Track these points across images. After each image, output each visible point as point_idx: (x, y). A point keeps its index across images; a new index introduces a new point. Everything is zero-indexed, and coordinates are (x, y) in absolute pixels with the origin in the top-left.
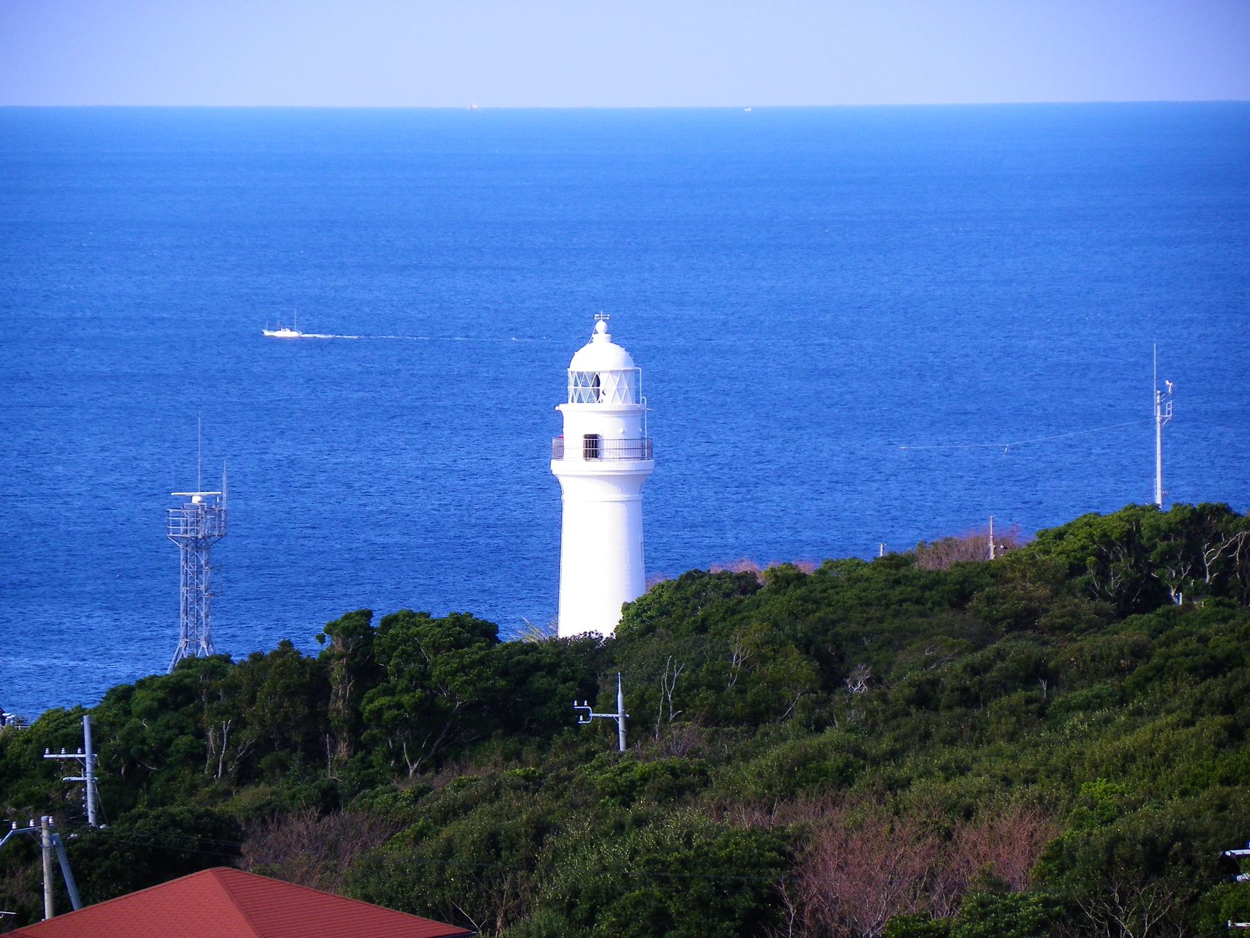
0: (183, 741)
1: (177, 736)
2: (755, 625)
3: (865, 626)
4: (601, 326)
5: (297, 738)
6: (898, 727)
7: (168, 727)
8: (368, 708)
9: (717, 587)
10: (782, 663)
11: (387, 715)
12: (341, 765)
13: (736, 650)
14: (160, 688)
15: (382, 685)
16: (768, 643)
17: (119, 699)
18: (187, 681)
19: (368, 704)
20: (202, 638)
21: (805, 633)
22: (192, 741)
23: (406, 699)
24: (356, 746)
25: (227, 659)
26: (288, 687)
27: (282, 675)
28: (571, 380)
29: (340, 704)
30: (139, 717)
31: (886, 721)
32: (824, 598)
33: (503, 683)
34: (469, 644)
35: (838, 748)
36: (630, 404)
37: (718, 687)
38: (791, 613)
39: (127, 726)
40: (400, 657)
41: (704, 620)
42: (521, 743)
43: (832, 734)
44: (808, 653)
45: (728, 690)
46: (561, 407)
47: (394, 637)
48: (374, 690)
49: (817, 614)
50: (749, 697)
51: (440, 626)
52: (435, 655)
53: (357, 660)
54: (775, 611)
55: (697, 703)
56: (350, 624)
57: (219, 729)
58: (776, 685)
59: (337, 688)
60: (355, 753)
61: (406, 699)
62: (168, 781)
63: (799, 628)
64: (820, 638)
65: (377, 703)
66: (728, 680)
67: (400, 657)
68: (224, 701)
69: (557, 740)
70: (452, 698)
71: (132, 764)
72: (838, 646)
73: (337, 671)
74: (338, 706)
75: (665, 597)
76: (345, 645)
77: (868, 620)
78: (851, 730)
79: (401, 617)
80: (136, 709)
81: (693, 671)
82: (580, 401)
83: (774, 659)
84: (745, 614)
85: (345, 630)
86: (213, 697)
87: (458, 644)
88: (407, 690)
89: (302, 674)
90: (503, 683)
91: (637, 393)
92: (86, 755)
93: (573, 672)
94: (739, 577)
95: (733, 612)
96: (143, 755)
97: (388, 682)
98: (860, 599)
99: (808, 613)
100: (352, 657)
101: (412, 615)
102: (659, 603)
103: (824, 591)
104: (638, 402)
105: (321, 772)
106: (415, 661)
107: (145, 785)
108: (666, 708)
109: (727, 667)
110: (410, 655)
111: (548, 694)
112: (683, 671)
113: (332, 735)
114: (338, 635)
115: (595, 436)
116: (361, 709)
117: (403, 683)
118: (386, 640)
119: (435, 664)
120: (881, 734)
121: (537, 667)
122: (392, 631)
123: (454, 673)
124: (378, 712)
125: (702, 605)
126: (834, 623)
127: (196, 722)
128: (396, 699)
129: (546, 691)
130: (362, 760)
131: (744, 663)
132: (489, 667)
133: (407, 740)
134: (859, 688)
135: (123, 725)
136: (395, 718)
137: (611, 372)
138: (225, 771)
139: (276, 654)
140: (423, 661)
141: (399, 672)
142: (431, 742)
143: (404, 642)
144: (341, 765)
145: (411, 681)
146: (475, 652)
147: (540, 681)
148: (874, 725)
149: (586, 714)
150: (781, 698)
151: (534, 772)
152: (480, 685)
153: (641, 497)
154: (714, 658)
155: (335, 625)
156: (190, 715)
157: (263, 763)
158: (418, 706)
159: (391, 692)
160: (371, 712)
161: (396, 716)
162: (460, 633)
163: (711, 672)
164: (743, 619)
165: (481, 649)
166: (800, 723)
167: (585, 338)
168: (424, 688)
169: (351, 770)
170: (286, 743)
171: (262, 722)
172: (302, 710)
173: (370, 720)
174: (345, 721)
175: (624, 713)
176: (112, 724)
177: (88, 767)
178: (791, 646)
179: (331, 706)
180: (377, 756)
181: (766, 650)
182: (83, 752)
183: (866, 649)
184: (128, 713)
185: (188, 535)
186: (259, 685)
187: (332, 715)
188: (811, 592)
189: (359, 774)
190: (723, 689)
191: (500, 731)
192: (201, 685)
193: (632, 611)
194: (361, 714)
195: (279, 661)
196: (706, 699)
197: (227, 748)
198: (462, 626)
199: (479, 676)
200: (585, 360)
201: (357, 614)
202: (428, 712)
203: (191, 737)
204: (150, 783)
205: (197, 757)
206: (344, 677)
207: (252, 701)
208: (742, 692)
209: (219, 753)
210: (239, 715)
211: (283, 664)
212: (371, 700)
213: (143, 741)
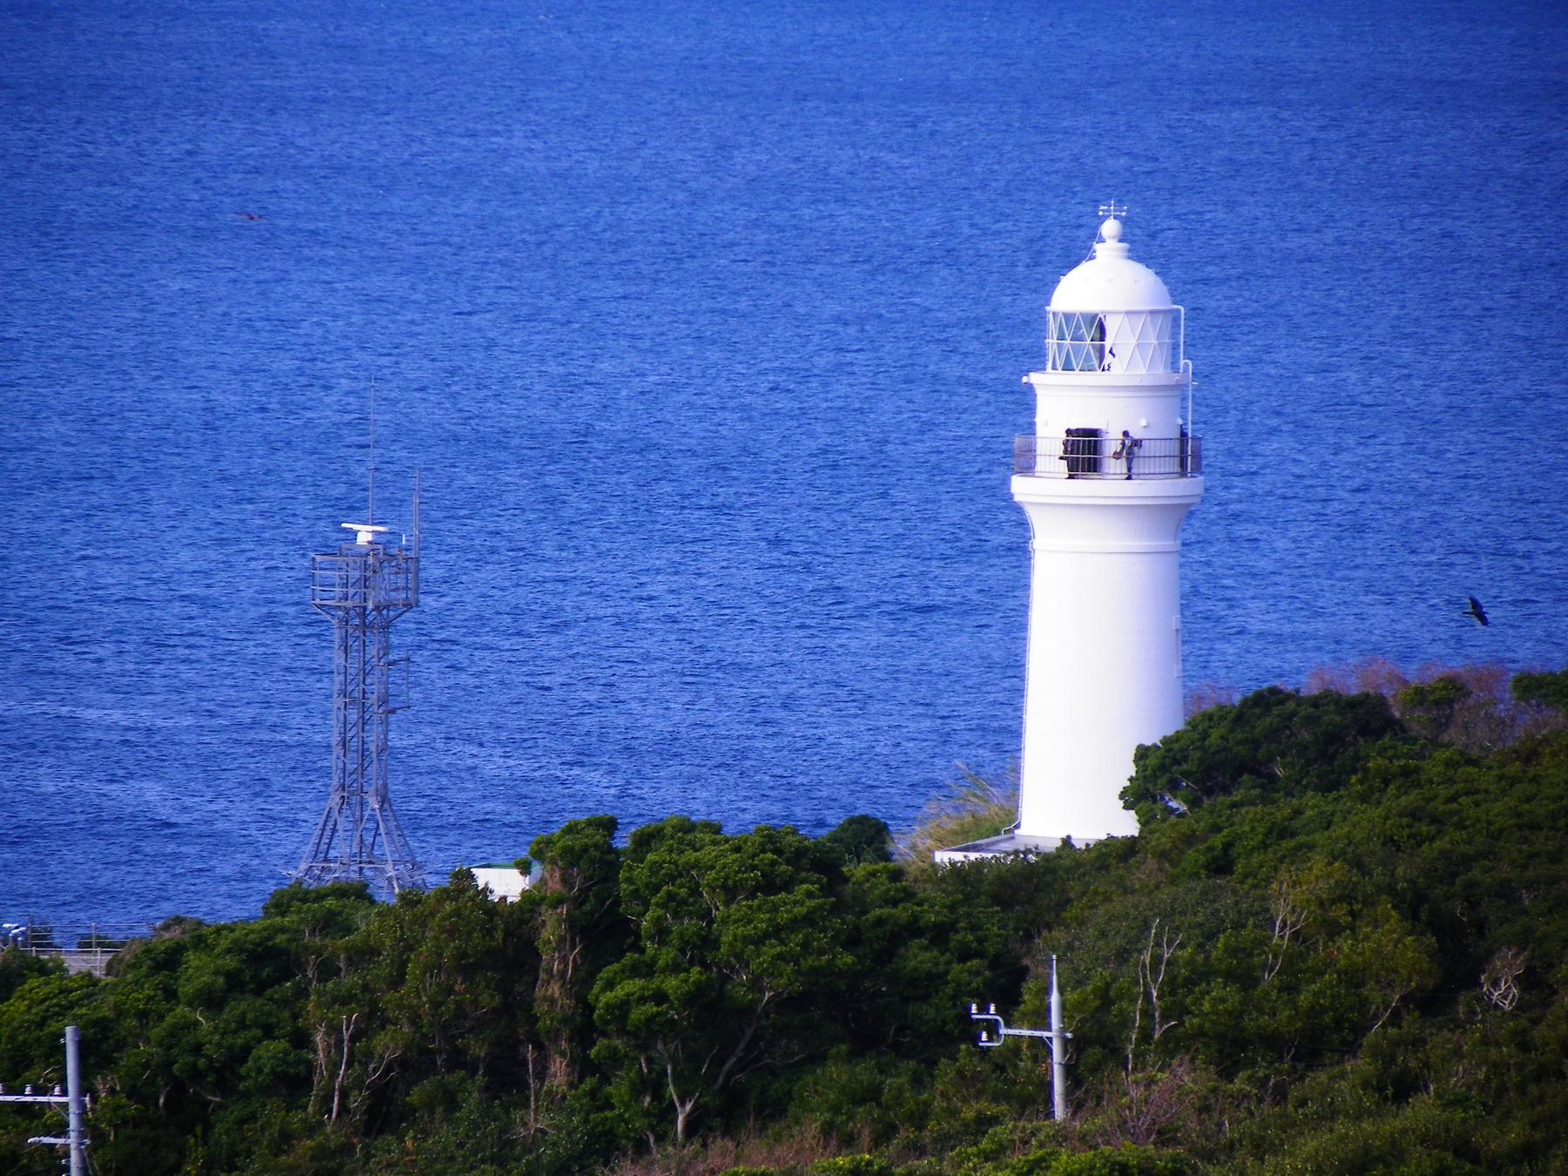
0: (269, 1052)
1: (259, 1041)
2: (1318, 863)
3: (1525, 867)
4: (1110, 228)
5: (478, 1049)
6: (1541, 1099)
7: (242, 1025)
8: (603, 999)
9: (1310, 721)
10: (1367, 938)
11: (637, 1014)
12: (555, 1102)
13: (1281, 911)
14: (229, 951)
15: (630, 957)
16: (1340, 899)
17: (157, 967)
18: (281, 939)
19: (603, 990)
20: (372, 790)
21: (1413, 882)
22: (286, 1053)
23: (672, 984)
24: (583, 1067)
25: (360, 893)
26: (464, 955)
27: (452, 933)
28: (1052, 326)
29: (555, 989)
30: (190, 1004)
31: (1521, 1089)
32: (1451, 814)
33: (849, 959)
34: (787, 886)
35: (1426, 1140)
36: (1161, 374)
37: (1245, 979)
38: (1389, 841)
39: (169, 1020)
40: (663, 905)
41: (1228, 846)
42: (881, 1072)
43: (1422, 1110)
44: (1415, 917)
45: (1263, 986)
46: (1034, 378)
47: (655, 868)
48: (616, 967)
49: (1437, 844)
50: (1304, 999)
51: (738, 849)
52: (727, 904)
53: (587, 907)
54: (1358, 835)
55: (1206, 1006)
56: (577, 842)
57: (334, 1030)
58: (1354, 978)
59: (551, 961)
60: (581, 1079)
61: (672, 984)
62: (241, 1122)
63: (1400, 871)
64: (1439, 891)
65: (620, 992)
66: (1264, 966)
67: (663, 905)
68: (349, 980)
69: (946, 1071)
70: (756, 984)
71: (178, 1086)
72: (1473, 904)
73: (551, 929)
74: (551, 994)
75: (1215, 737)
76: (566, 881)
77: (1532, 856)
78: (1459, 1102)
79: (668, 831)
80: (186, 989)
81: (1201, 946)
82: (1067, 367)
83: (1353, 929)
84: (1302, 839)
85: (567, 851)
86: (328, 970)
87: (769, 885)
88: (675, 968)
89: (489, 933)
90: (849, 959)
91: (1175, 347)
92: (67, 1099)
93: (980, 941)
94: (1354, 704)
95: (1284, 833)
96: (196, 1075)
97: (642, 951)
98: (1519, 816)
99: (1419, 840)
100: (579, 901)
101: (687, 827)
102: (1202, 748)
103: (1453, 799)
104: (1176, 370)
105: (517, 1115)
106: (690, 914)
107: (199, 1130)
108: (1147, 1014)
109: (1262, 943)
110: (684, 902)
111: (936, 979)
112: (1182, 946)
113: (539, 1047)
114: (553, 862)
115: (1093, 433)
116: (591, 998)
117: (667, 955)
118: (641, 873)
119: (724, 922)
120: (1508, 1115)
121: (913, 929)
122: (650, 857)
123: (759, 941)
124: (623, 1007)
125: (1283, 755)
126: (1467, 861)
127: (295, 1017)
128: (655, 983)
129: (931, 976)
130: (593, 1094)
131: (1295, 936)
132: (824, 930)
133: (673, 1059)
134: (1503, 993)
135: (161, 1018)
136: (651, 1019)
137: (1128, 313)
138: (343, 1109)
139: (444, 895)
140: (706, 915)
141: (661, 934)
142: (718, 1062)
143: (672, 878)
144: (555, 1102)
145: (682, 951)
146: (802, 897)
147: (918, 957)
148: (1502, 1090)
149: (992, 1028)
150: (1363, 1004)
151: (869, 1163)
152: (809, 962)
153: (1171, 544)
154: (1239, 926)
155: (549, 842)
156: (285, 1003)
157: (415, 1096)
158: (692, 999)
159: (646, 970)
160: (609, 1007)
161: (658, 1014)
162: (773, 863)
163: (1232, 951)
164: (1299, 847)
165: (810, 895)
166: (1366, 1085)
167: (1076, 253)
168: (706, 967)
169: (572, 1112)
170: (458, 1060)
171: (415, 1021)
172: (489, 1000)
173: (607, 1023)
174: (565, 1021)
175: (1063, 1030)
176: (143, 1015)
177: (73, 1122)
178: (1385, 905)
179: (539, 992)
180: (618, 1089)
181: (1340, 913)
182: (64, 1093)
183: (1525, 912)
184: (171, 994)
185: (349, 604)
186: (411, 948)
187: (541, 1008)
188: (1429, 800)
189: (586, 1121)
190: (1256, 981)
191: (844, 1048)
192: (306, 948)
193: (1152, 761)
194: (592, 1009)
195: (448, 907)
196: (1223, 1000)
197: (349, 1065)
198: (778, 852)
199: (805, 945)
200: (1076, 292)
201: (589, 823)
202: (709, 1006)
203: (283, 1044)
204: (208, 1127)
205: (293, 1083)
206: (562, 939)
207: (397, 981)
208: (1290, 989)
209: (333, 1075)
210: (374, 1004)
211: (457, 913)
212: (610, 985)
213: (197, 1049)
